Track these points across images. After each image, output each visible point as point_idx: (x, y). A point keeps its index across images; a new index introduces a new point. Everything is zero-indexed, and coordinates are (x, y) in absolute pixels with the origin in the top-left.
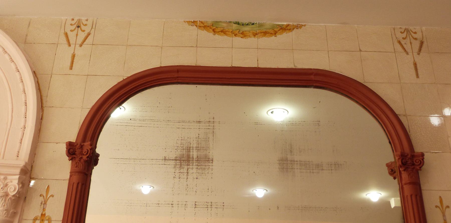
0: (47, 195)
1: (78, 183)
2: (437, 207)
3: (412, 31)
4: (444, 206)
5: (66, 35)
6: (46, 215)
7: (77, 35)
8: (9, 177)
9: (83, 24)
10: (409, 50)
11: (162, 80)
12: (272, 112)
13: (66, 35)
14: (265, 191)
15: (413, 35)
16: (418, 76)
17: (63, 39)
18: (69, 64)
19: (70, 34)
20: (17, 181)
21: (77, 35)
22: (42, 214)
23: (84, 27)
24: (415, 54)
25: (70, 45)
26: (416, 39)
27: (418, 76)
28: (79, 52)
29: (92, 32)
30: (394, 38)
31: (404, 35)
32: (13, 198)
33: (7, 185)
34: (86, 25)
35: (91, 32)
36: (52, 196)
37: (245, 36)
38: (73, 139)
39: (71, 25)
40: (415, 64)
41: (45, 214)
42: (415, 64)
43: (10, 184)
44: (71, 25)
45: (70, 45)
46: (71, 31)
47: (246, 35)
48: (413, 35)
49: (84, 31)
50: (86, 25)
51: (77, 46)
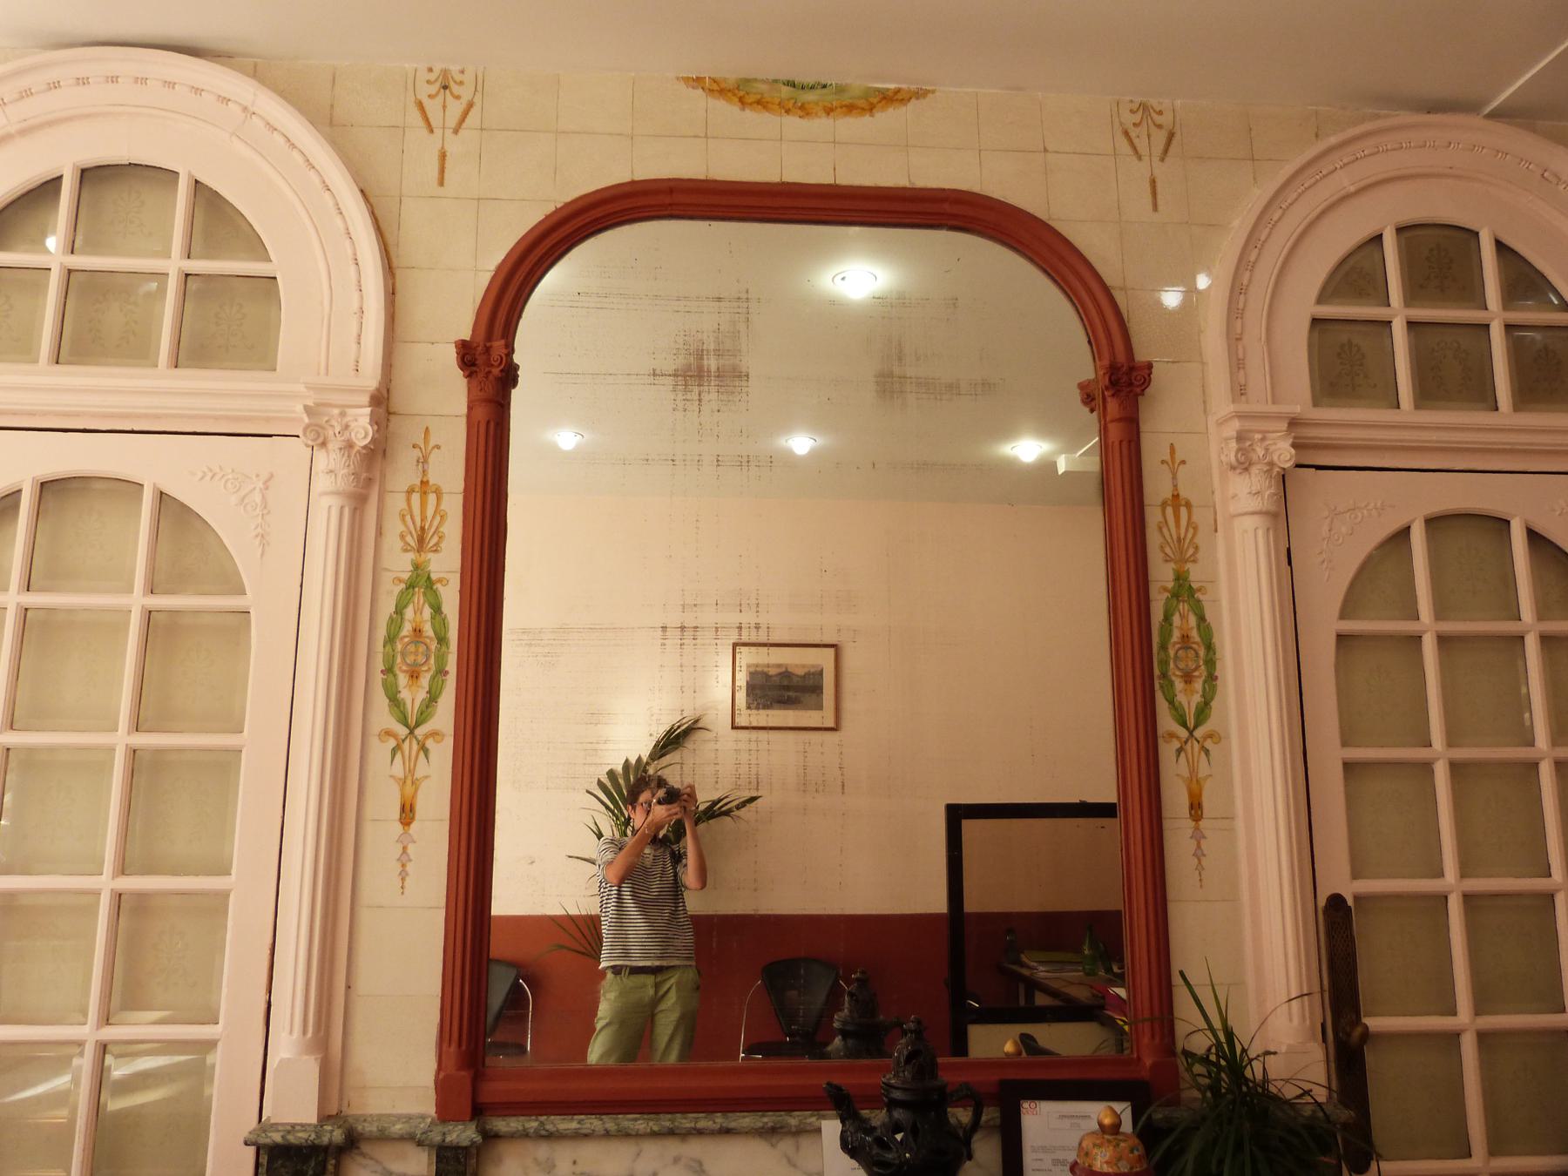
0: (1173, 463)
1: (488, 422)
4: (432, 444)
6: (431, 483)
7: (444, 107)
8: (350, 411)
9: (455, 82)
12: (843, 279)
15: (1153, 114)
17: (414, 117)
20: (367, 419)
21: (444, 107)
22: (1173, 495)
24: (1156, 160)
25: (1140, 158)
26: (1160, 127)
29: (477, 100)
31: (1137, 118)
32: (364, 451)
33: (347, 427)
34: (461, 83)
37: (808, 114)
40: (1153, 183)
41: (1178, 495)
42: (1153, 183)
43: (353, 425)
45: (432, 131)
49: (458, 97)
50: (461, 83)
51: (449, 132)
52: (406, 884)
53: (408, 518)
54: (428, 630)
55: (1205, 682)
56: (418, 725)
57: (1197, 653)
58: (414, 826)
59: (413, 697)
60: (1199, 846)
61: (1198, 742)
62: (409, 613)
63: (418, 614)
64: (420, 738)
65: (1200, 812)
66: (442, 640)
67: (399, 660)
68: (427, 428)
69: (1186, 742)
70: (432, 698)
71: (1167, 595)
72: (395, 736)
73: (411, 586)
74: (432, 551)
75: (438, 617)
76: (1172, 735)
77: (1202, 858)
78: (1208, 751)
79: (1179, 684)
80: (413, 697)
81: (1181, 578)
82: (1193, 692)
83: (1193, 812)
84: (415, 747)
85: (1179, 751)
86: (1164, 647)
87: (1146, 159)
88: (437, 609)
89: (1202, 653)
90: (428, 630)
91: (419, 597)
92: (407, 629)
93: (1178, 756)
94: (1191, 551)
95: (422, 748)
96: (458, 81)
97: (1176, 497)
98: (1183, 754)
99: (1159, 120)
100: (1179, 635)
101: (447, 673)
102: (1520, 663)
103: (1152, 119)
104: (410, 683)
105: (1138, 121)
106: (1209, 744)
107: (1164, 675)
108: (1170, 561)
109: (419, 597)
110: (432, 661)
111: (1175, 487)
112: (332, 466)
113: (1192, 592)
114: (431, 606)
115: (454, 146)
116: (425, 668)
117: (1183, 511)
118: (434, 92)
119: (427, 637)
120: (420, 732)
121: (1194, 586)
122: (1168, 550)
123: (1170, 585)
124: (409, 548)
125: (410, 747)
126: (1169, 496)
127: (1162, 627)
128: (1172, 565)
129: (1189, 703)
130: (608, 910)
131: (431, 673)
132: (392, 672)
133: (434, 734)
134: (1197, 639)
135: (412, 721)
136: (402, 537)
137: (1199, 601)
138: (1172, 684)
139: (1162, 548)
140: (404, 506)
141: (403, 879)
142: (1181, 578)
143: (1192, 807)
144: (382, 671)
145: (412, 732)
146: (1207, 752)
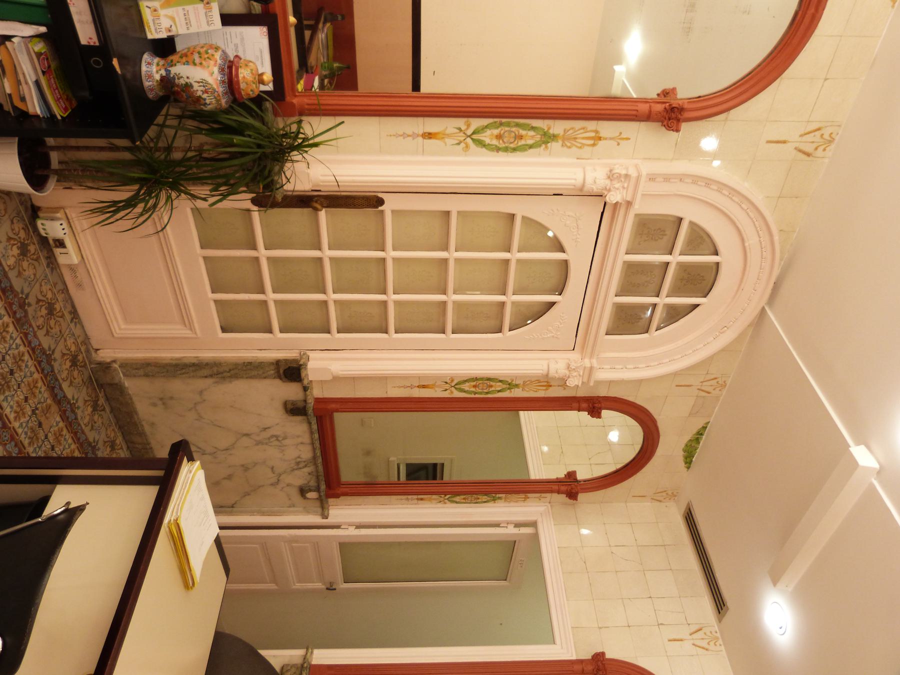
2: (621, 133)
10: (695, 636)
15: (823, 147)
16: (769, 142)
22: (601, 137)
24: (797, 145)
28: (687, 646)
36: (618, 144)
42: (784, 142)
51: (692, 642)
52: (392, 137)
60: (409, 136)
62: (531, 133)
65: (426, 138)
66: (487, 393)
68: (630, 139)
69: (464, 133)
72: (467, 129)
74: (563, 144)
76: (469, 126)
77: (402, 137)
79: (496, 132)
81: (554, 137)
83: (427, 134)
85: (460, 129)
86: (517, 125)
90: (522, 142)
92: (523, 132)
94: (569, 144)
96: (716, 643)
97: (600, 139)
98: (458, 131)
99: (712, 643)
100: (523, 134)
106: (463, 145)
107: (501, 124)
110: (486, 382)
111: (606, 139)
112: (597, 181)
113: (546, 143)
114: (533, 144)
115: (687, 646)
117: (591, 142)
119: (518, 143)
120: (469, 140)
121: (549, 145)
122: (571, 132)
123: (551, 131)
126: (601, 135)
127: (529, 125)
129: (485, 136)
134: (520, 144)
138: (497, 128)
139: (572, 128)
141: (394, 135)
142: (554, 137)
143: (430, 134)
145: (469, 136)
146: (458, 144)
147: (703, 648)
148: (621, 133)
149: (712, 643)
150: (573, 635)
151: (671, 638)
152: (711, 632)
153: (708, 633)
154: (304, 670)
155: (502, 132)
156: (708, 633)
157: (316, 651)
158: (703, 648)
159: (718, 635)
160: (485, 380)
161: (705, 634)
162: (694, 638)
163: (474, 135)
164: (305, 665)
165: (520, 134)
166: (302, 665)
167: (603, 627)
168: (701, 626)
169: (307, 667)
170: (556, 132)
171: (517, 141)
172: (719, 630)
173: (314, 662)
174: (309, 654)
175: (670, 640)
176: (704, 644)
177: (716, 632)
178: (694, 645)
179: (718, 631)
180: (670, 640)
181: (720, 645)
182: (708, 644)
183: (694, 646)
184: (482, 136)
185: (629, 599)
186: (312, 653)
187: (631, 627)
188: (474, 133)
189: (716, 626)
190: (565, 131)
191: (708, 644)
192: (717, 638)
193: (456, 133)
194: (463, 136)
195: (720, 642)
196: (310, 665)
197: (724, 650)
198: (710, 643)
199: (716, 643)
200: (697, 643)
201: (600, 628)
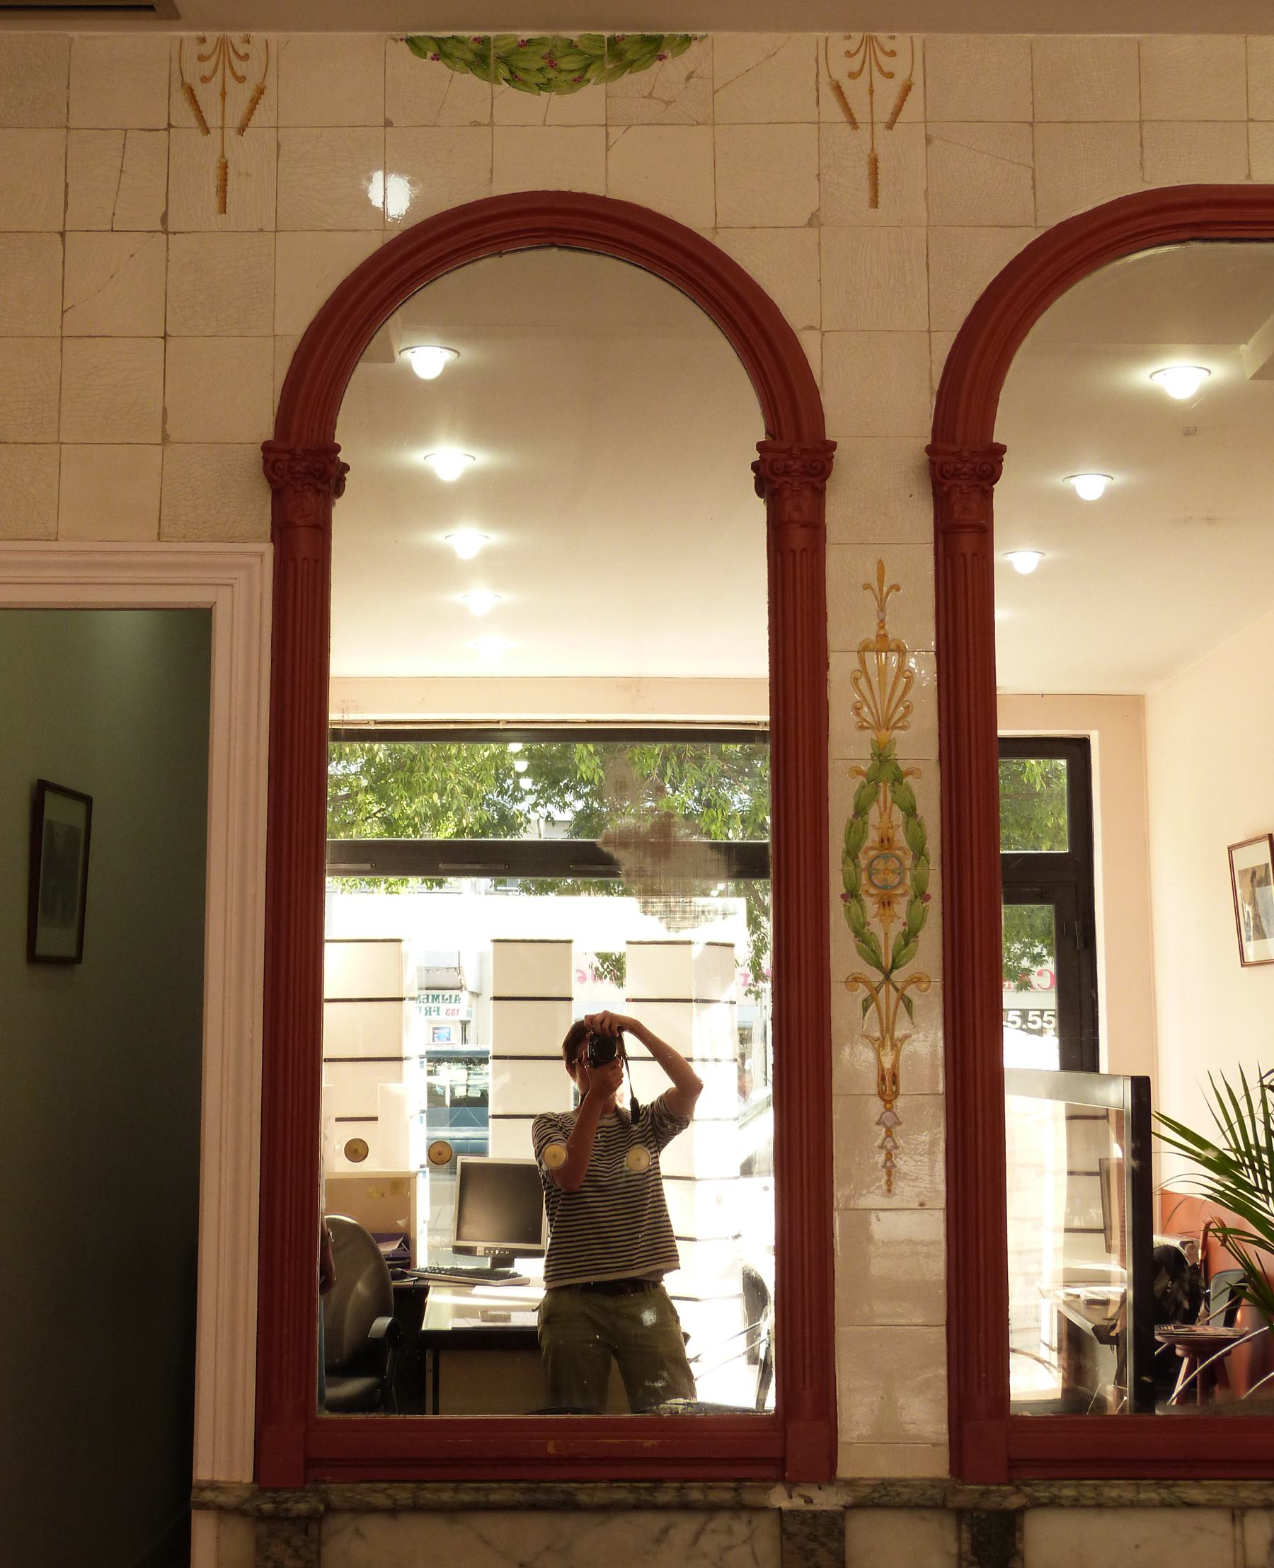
0: (881, 590)
3: (882, 50)
4: (888, 582)
5: (838, 89)
7: (223, 94)
10: (212, 119)
11: (483, 245)
13: (838, 89)
14: (1038, 556)
15: (884, 60)
16: (874, 203)
18: (865, 195)
19: (847, 85)
21: (223, 94)
22: (878, 635)
23: (244, 64)
25: (207, 131)
27: (874, 203)
28: (242, 152)
29: (271, 83)
30: (176, 75)
34: (892, 54)
35: (266, 83)
36: (896, 588)
38: (762, 437)
39: (849, 54)
41: (885, 636)
42: (874, 163)
44: (849, 54)
46: (853, 76)
47: (520, 74)
48: (884, 60)
49: (890, 75)
50: (892, 54)
51: (231, 133)
53: (862, 682)
54: (900, 838)
55: (911, 903)
56: (895, 966)
57: (901, 863)
58: (900, 1103)
59: (886, 932)
61: (897, 990)
62: (874, 815)
63: (885, 817)
64: (899, 985)
67: (864, 880)
70: (910, 936)
71: (861, 779)
72: (866, 983)
73: (873, 779)
74: (900, 728)
75: (912, 822)
78: (910, 1001)
80: (886, 932)
82: (894, 916)
84: (894, 995)
87: (215, 133)
88: (911, 812)
89: (908, 863)
90: (900, 838)
91: (885, 793)
92: (873, 837)
93: (865, 1009)
95: (902, 998)
96: (242, 53)
99: (241, 67)
101: (927, 898)
102: (367, 867)
103: (231, 65)
104: (882, 911)
105: (853, 51)
106: (911, 991)
108: (868, 728)
109: (885, 793)
113: (898, 778)
115: (242, 152)
116: (900, 891)
118: (856, 69)
120: (898, 976)
121: (903, 766)
124: (865, 724)
125: (888, 997)
128: (869, 734)
129: (886, 934)
130: (556, 1199)
131: (907, 898)
132: (856, 897)
133: (916, 980)
135: (887, 961)
136: (857, 710)
137: (908, 788)
140: (857, 665)
144: (843, 896)
146: (909, 1005)
147: (255, 102)
148: (867, 586)
149: (241, 67)
150: (184, 538)
151: (214, 201)
152: (201, 58)
153: (207, 68)
154: (287, 1510)
155: (873, 891)
156: (207, 68)
157: (202, 1472)
158: (255, 102)
159: (212, 36)
160: (914, 879)
161: (205, 80)
162: (220, 124)
163: (883, 960)
164: (268, 1507)
165: (877, 845)
166: (261, 1517)
167: (164, 431)
168: (177, 84)
169: (274, 1502)
170: (867, 752)
171: (897, 852)
172: (201, 29)
173: (243, 1473)
174: (222, 1499)
175: (223, 208)
176: (240, 96)
177: (203, 40)
178: (241, 130)
179: (200, 34)
180: (223, 208)
181: (248, 41)
182: (241, 79)
183: (248, 131)
184: (886, 947)
185: (63, 312)
186: (213, 1486)
187: (169, 332)
188: (878, 965)
189: (184, 34)
190: (862, 728)
191: (241, 79)
192: (223, 44)
193: (879, 1009)
194: (887, 992)
195: (236, 36)
196: (262, 1490)
197: (266, 35)
198: (239, 73)
199: (242, 53)
200: (235, 119)
201: (165, 439)
